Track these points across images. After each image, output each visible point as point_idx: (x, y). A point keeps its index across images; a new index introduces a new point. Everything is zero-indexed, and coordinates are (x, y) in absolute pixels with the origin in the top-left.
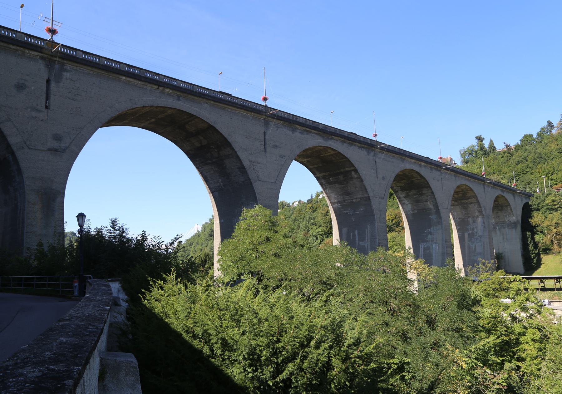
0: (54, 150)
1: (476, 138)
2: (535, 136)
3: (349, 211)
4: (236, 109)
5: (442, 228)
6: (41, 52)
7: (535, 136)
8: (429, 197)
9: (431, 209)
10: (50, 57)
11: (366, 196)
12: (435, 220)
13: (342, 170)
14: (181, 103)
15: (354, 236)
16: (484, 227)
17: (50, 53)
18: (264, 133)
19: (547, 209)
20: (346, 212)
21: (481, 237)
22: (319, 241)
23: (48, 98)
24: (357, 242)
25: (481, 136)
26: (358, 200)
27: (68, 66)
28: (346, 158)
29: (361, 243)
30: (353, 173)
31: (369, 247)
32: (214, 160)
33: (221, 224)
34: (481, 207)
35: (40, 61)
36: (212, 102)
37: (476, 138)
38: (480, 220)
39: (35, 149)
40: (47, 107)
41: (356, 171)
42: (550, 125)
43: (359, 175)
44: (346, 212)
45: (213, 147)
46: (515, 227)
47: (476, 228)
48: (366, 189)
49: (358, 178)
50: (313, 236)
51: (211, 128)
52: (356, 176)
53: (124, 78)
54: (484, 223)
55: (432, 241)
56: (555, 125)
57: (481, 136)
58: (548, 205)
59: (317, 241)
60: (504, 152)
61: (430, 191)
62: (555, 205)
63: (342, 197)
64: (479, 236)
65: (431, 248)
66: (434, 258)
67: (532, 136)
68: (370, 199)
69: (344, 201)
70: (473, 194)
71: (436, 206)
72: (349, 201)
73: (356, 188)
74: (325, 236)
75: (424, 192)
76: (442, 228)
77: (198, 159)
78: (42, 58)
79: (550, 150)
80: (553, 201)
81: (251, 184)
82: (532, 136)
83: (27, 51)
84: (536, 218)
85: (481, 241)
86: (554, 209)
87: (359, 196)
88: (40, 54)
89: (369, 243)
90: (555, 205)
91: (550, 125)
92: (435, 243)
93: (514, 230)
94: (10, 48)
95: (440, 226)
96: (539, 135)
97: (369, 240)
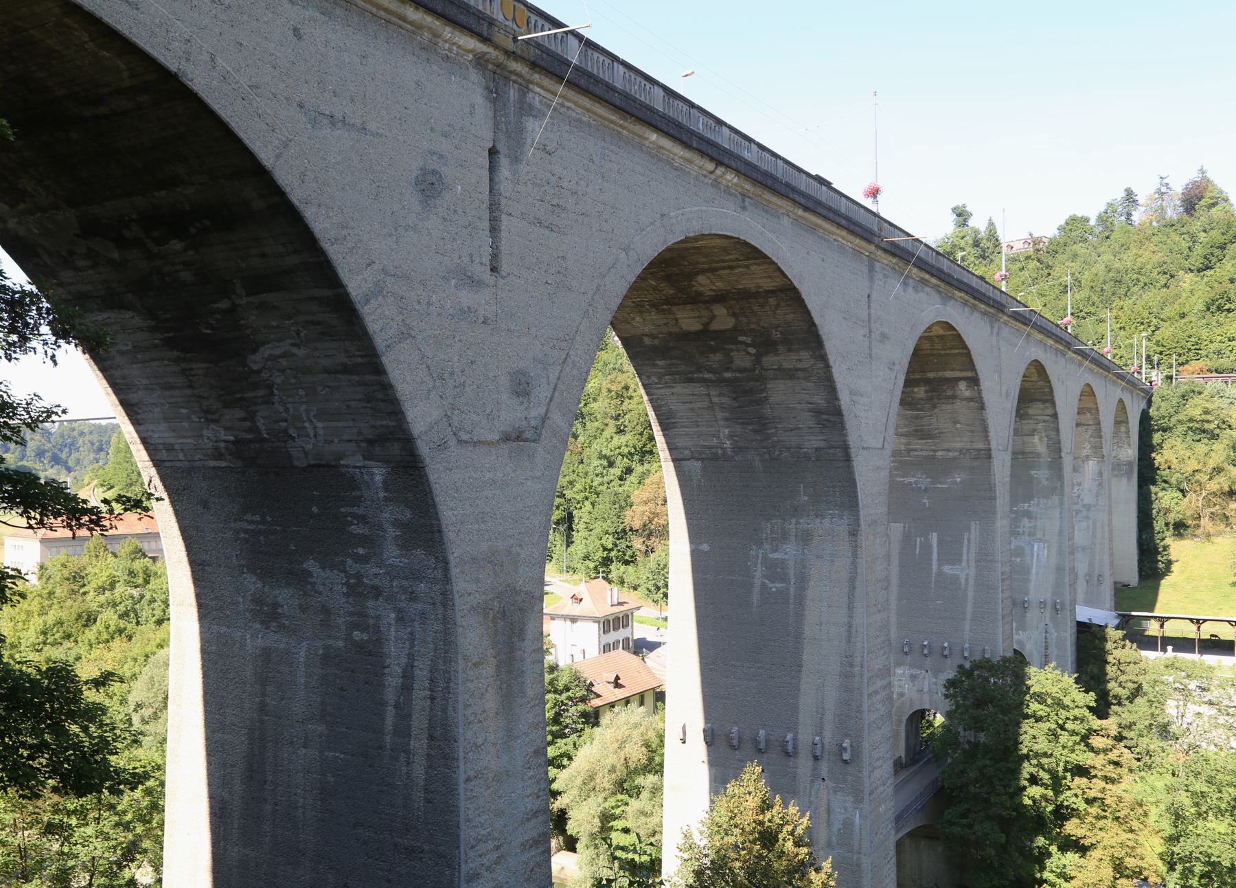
0: (515, 437)
1: (954, 210)
2: (1093, 222)
3: (917, 479)
4: (833, 229)
5: (1061, 503)
6: (486, 40)
7: (1093, 222)
8: (1040, 426)
9: (1038, 455)
10: (502, 58)
11: (981, 446)
12: (1046, 483)
13: (931, 375)
14: (746, 217)
15: (927, 547)
16: (1100, 484)
17: (510, 46)
18: (869, 296)
19: (1190, 428)
20: (907, 480)
21: (1088, 507)
22: (616, 471)
23: (494, 230)
24: (935, 566)
25: (964, 206)
26: (951, 454)
27: (547, 94)
28: (966, 348)
29: (947, 569)
30: (962, 386)
31: (971, 581)
32: (727, 375)
33: (696, 556)
34: (1101, 437)
35: (475, 76)
36: (800, 212)
37: (954, 210)
38: (1091, 466)
39: (476, 444)
40: (494, 269)
41: (974, 381)
42: (1130, 198)
43: (979, 392)
44: (907, 480)
45: (749, 340)
46: (1128, 474)
47: (1079, 485)
48: (985, 430)
49: (971, 399)
50: (602, 456)
51: (790, 294)
52: (968, 394)
53: (654, 137)
54: (1100, 474)
55: (1032, 534)
56: (1141, 198)
57: (964, 206)
58: (1191, 420)
59: (612, 471)
60: (1028, 258)
61: (1050, 411)
62: (1208, 422)
63: (903, 440)
64: (1084, 506)
65: (1027, 551)
66: (1033, 577)
67: (1087, 220)
68: (989, 457)
69: (909, 451)
70: (1091, 405)
71: (1056, 448)
72: (924, 453)
73: (955, 423)
74: (636, 458)
75: (1031, 411)
76: (1061, 503)
77: (660, 363)
78: (480, 61)
79: (1139, 265)
80: (1207, 412)
81: (848, 458)
82: (1087, 220)
83: (447, 32)
84: (1172, 454)
85: (1087, 518)
86: (1204, 431)
87: (958, 445)
88: (481, 47)
89: (972, 571)
90: (1208, 422)
91: (1130, 198)
92: (1040, 540)
93: (1124, 480)
94: (403, 18)
95: (1056, 499)
96: (1103, 220)
97: (972, 563)
